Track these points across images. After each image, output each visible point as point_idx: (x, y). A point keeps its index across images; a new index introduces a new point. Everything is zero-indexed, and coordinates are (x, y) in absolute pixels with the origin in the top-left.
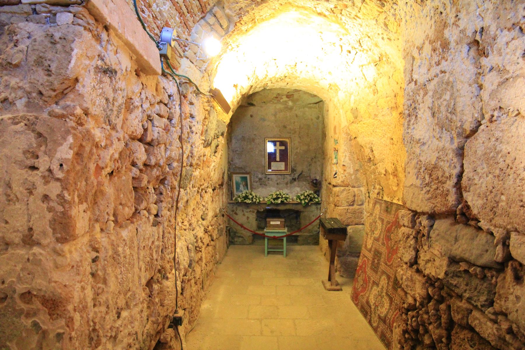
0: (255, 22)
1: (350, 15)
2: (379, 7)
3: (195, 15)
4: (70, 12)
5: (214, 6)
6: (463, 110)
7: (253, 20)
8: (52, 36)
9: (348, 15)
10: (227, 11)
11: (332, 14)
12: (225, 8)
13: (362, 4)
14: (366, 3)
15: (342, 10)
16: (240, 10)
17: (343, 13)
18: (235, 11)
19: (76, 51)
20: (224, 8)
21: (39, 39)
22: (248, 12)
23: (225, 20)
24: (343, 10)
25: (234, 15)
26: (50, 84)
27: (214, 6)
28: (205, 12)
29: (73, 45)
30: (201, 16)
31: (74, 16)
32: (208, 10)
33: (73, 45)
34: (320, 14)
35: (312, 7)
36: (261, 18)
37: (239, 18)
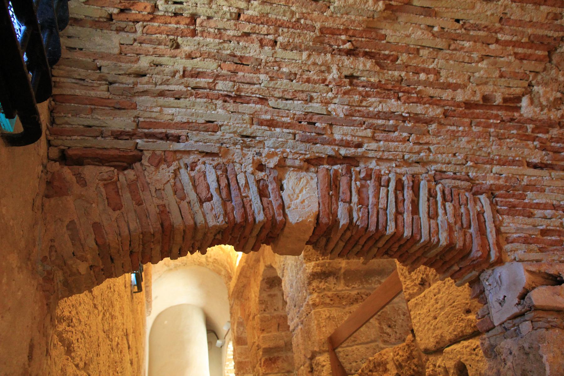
4: (526, 320)
6: (47, 196)
8: (523, 347)
19: (545, 357)
21: (516, 354)
29: (540, 352)
31: (532, 322)
33: (540, 352)
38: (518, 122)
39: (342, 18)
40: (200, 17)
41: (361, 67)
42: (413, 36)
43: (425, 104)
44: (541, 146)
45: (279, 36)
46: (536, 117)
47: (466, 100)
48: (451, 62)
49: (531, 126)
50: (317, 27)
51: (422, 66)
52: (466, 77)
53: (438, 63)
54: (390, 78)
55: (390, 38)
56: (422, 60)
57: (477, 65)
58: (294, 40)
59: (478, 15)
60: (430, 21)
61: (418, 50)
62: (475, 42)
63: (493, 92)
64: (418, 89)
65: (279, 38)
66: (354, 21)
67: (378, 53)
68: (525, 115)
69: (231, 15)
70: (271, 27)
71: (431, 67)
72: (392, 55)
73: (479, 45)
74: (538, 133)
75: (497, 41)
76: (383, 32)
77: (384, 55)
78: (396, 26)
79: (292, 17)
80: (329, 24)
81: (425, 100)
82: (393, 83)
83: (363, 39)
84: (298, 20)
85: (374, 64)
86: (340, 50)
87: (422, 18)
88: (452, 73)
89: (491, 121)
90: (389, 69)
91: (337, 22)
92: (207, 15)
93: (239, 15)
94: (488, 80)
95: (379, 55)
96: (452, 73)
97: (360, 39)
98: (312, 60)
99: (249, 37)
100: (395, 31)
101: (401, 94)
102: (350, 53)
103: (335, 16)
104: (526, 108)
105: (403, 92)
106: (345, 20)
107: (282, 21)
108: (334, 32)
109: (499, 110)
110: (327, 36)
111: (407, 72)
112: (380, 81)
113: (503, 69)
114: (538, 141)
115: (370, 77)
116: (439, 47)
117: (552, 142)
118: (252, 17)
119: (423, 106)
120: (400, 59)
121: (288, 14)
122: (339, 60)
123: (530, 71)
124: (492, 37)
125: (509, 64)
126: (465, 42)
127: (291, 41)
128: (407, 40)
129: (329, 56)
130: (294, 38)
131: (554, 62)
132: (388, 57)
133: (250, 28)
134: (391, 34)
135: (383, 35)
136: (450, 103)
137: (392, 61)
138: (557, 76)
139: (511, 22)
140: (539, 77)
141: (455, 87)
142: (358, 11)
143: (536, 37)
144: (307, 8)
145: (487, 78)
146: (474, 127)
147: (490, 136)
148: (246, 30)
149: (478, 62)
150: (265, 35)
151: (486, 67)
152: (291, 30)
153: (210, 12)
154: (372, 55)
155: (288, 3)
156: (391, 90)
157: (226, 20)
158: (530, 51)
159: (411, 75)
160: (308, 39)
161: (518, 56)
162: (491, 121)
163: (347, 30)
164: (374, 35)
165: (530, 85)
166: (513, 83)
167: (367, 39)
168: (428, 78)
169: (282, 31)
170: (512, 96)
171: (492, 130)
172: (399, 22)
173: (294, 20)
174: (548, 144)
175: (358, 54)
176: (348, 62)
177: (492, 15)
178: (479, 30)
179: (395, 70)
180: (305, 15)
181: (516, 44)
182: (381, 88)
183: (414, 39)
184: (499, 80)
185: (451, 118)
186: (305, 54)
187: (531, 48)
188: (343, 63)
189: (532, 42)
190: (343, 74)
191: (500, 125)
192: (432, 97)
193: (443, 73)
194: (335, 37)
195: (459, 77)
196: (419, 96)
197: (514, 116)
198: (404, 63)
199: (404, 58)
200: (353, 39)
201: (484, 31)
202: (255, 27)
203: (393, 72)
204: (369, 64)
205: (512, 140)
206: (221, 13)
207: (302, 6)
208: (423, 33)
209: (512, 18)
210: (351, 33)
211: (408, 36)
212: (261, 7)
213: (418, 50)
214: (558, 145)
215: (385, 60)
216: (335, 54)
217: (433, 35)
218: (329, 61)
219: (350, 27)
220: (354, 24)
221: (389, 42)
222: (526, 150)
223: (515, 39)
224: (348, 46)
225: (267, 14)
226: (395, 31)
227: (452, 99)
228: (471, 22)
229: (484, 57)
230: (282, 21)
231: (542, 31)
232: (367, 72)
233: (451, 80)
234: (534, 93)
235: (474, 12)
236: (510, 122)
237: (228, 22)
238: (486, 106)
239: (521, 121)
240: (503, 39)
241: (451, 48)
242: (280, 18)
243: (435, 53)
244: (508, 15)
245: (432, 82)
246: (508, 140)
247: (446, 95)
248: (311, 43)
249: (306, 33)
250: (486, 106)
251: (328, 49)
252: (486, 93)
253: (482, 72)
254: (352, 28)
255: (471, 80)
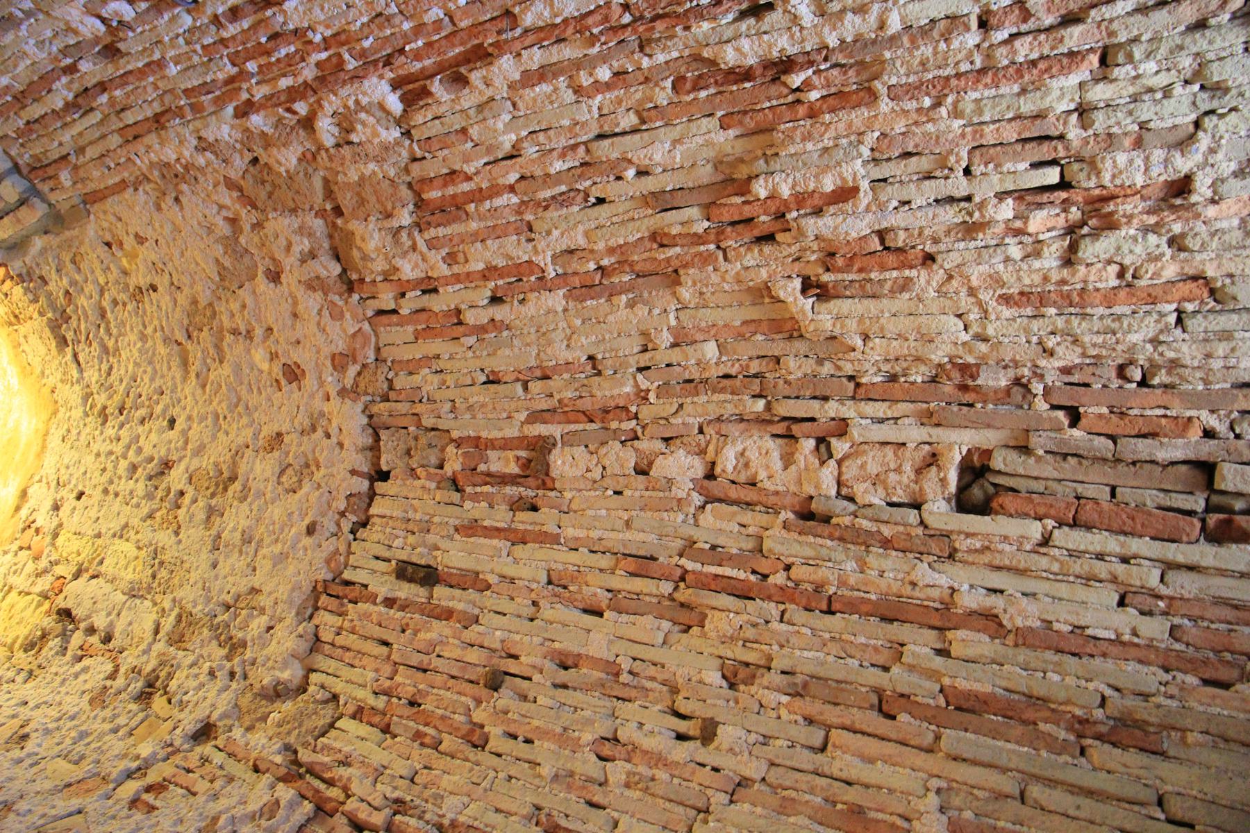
0: (11, 324)
1: (15, 573)
2: (26, 638)
3: (22, 145)
5: (50, 205)
7: (16, 317)
9: (14, 568)
10: (38, 243)
11: (21, 526)
12: (45, 237)
13: (39, 595)
14: (40, 605)
15: (29, 548)
16: (42, 278)
17: (20, 553)
18: (38, 265)
20: (46, 233)
22: (36, 300)
23: (10, 232)
24: (28, 552)
25: (28, 260)
26: (600, 272)
27: (50, 205)
28: (32, 176)
30: (20, 162)
32: (40, 186)
34: (24, 494)
35: (43, 472)
36: (22, 340)
37: (20, 275)
38: (375, 62)
39: (836, 138)
40: (1234, 17)
41: (745, 44)
42: (667, 146)
43: (565, 21)
44: (305, 35)
45: (978, 46)
46: (356, 85)
47: (491, 63)
48: (566, 122)
49: (350, 67)
50: (887, 100)
51: (616, 93)
52: (520, 104)
53: (589, 111)
54: (669, 43)
55: (710, 126)
56: (624, 104)
57: (517, 135)
58: (935, 48)
59: (571, 224)
60: (649, 184)
61: (643, 122)
62: (548, 175)
63: (458, 98)
64: (598, 45)
65: (977, 40)
66: (803, 140)
67: (722, 85)
68: (375, 80)
69: (1130, 58)
70: (1006, 62)
71: (599, 98)
72: (689, 92)
73: (538, 172)
74: (330, 57)
75: (512, 189)
76: (731, 133)
77: (706, 87)
78: (711, 154)
79: (955, 104)
80: (859, 116)
81: (570, 30)
82: (658, 35)
83: (768, 104)
84: (937, 104)
85: (720, 61)
86: (811, 63)
87: (668, 184)
88: (552, 103)
89: (420, 43)
90: (680, 62)
91: (841, 126)
92: (1207, 32)
93: (1103, 61)
94: (480, 117)
95: (716, 82)
96: (552, 103)
97: (774, 103)
98: (872, 18)
99: (1063, 12)
100: (708, 144)
101: (627, 18)
102: (786, 65)
103: (853, 138)
104: (379, 90)
105: (625, 26)
106: (826, 136)
107: (981, 87)
108: (839, 99)
109: (423, 68)
110: (855, 87)
111: (639, 69)
112: (687, 28)
113: (470, 145)
114: (318, 45)
115: (713, 28)
116: (607, 142)
117: (297, 51)
118: (1065, 71)
119: (566, 14)
120: (669, 90)
121: (968, 107)
122: (803, 41)
123: (424, 158)
124: (525, 194)
125: (467, 160)
126: (565, 168)
127: (942, 45)
128: (676, 132)
129: (832, 41)
130: (935, 53)
131: (404, 188)
132: (696, 88)
133: (1066, 40)
134: (713, 135)
135: (729, 127)
136: (517, 46)
137: (684, 78)
138: (381, 167)
139: (511, 229)
140: (405, 154)
141: (531, 78)
142: (805, 164)
143: (456, 220)
144: (925, 134)
145: (485, 119)
146: (442, 16)
147: (401, 12)
148: (1076, 31)
149: (520, 140)
150: (1019, 34)
151: (501, 139)
152: (949, 71)
153: (1200, 42)
154: (732, 77)
155: (975, 132)
156: (653, 19)
157: (1143, 38)
158: (451, 190)
159: (628, 66)
160: (898, 64)
161: (462, 176)
162: (420, 43)
163: (813, 114)
164: (750, 123)
165: (407, 134)
166: (436, 128)
167: (758, 107)
168: (591, 75)
169: (972, 63)
170: (421, 103)
171: (406, 26)
172: (708, 162)
173: (950, 100)
174: (299, 45)
175: (765, 68)
176: (780, 46)
177: (549, 233)
178: (553, 197)
179: (667, 63)
180: (924, 119)
181: (479, 196)
182: (678, 16)
183: (661, 142)
184: (464, 124)
185: (495, 14)
186: (895, 24)
187: (454, 196)
188: (792, 37)
189: (458, 208)
190: (780, 10)
191: (401, 42)
192: (560, 41)
193: (569, 96)
194: (833, 90)
195: (535, 100)
196: (588, 34)
197: (391, 71)
198: (657, 85)
199: (663, 94)
200: (790, 98)
201: (545, 200)
202: (1052, 49)
203: (668, 58)
204: (730, 57)
205: (358, 24)
206: (1163, 51)
207: (938, 137)
208: (650, 159)
209: (515, 237)
210: (802, 110)
211: (676, 142)
212: (1046, 103)
213: (643, 122)
214: (283, 52)
215: (700, 77)
216: (819, 50)
217: (630, 162)
218: (826, 30)
219: (809, 122)
220: (803, 133)
221: (709, 115)
222: (322, 18)
223: (487, 204)
224: (796, 80)
225: (1024, 91)
226: (708, 144)
227: (519, 55)
228: (576, 209)
229: (515, 153)
230: (981, 87)
231: (456, 232)
232: (725, 38)
233: (545, 88)
234: (392, 124)
235: (581, 228)
236: (389, 55)
237: (1136, 32)
238: (451, 66)
239: (372, 69)
240: (505, 196)
241: (582, 148)
242: (986, 93)
243: (606, 128)
244: (523, 239)
245: (579, 69)
246: (365, 19)
247: (535, 58)
248: (887, 55)
249: (908, 75)
250: (451, 66)
251: (840, 56)
252: (467, 91)
253: (500, 126)
254: (802, 123)
255: (509, 103)
